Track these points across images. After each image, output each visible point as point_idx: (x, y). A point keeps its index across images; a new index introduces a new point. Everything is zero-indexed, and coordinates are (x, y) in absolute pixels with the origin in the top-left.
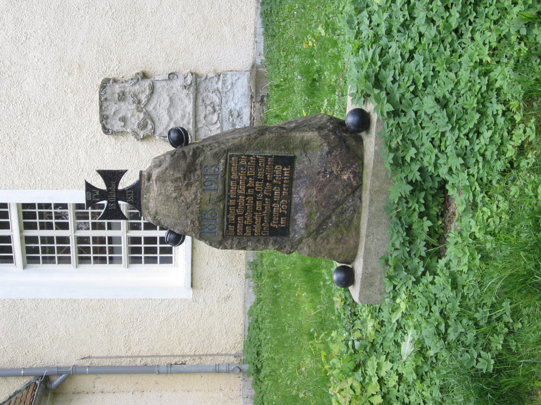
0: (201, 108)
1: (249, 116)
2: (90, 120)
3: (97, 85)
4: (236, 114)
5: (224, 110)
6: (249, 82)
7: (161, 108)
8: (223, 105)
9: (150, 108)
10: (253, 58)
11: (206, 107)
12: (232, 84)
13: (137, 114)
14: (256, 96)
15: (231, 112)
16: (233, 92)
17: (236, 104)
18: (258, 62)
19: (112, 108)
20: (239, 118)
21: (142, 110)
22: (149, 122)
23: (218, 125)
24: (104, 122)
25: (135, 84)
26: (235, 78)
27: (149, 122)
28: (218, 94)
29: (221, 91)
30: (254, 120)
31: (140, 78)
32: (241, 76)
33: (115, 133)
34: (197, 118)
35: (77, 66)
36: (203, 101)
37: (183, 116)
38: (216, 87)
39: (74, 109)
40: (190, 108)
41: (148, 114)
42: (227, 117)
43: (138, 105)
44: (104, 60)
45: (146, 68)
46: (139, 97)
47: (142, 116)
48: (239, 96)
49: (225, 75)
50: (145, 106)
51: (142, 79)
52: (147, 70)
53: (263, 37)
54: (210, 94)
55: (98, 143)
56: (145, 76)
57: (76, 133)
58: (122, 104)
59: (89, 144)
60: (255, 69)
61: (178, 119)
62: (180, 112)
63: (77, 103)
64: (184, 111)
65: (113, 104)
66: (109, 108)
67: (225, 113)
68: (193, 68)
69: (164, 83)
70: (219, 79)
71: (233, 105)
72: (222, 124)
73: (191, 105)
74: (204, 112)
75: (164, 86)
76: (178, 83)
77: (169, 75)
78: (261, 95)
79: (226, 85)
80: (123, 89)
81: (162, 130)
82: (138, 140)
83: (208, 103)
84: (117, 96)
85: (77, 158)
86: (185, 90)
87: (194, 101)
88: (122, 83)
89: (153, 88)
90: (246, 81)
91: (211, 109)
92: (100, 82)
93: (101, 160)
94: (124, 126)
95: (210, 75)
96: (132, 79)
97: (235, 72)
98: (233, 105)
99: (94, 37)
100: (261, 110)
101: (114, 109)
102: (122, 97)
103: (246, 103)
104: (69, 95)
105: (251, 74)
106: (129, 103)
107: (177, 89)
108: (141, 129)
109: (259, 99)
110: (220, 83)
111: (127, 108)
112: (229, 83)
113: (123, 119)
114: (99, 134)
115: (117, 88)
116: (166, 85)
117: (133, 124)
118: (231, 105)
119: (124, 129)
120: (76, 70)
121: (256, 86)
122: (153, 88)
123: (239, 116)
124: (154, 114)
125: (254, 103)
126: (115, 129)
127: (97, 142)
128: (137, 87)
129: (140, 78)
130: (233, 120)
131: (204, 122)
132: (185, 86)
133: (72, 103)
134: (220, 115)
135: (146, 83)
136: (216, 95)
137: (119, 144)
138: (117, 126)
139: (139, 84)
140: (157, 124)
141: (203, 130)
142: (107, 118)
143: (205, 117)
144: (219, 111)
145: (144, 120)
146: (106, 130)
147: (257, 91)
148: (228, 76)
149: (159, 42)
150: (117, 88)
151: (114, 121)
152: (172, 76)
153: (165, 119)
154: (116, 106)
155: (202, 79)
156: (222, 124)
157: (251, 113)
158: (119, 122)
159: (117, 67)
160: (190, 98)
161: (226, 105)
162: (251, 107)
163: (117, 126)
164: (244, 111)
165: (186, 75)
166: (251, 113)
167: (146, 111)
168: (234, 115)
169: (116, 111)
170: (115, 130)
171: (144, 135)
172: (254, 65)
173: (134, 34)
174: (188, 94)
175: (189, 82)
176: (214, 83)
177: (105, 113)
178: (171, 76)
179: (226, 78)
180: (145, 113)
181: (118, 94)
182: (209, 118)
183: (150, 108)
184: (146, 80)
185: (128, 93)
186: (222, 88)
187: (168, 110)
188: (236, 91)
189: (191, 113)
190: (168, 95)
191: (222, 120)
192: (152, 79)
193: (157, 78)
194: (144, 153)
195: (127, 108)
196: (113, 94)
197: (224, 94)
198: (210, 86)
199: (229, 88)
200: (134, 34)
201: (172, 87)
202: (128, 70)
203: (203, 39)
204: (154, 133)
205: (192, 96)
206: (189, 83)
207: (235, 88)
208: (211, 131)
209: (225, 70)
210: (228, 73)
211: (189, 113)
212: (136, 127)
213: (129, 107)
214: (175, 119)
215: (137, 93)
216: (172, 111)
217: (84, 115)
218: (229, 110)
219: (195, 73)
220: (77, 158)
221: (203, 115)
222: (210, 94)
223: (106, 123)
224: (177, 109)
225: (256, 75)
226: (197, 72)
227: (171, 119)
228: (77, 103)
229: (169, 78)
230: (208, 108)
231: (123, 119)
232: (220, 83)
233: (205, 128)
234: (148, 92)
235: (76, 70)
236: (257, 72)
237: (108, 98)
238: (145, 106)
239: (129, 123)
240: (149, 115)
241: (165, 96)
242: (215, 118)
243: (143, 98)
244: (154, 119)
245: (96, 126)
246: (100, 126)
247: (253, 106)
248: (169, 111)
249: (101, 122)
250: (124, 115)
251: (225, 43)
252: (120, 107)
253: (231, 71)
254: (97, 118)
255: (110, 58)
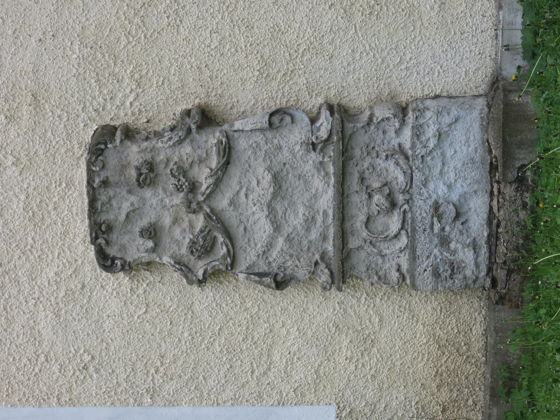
0: (357, 199)
1: (485, 216)
2: (66, 233)
3: (80, 144)
4: (450, 211)
5: (418, 202)
6: (485, 129)
7: (250, 202)
8: (415, 190)
9: (222, 202)
10: (495, 60)
11: (370, 196)
12: (440, 136)
13: (186, 218)
14: (505, 167)
15: (436, 206)
16: (443, 155)
17: (450, 187)
18: (510, 72)
19: (122, 205)
20: (458, 224)
21: (201, 208)
22: (220, 239)
23: (404, 240)
24: (101, 241)
25: (180, 142)
26: (447, 119)
27: (220, 239)
28: (402, 161)
29: (410, 153)
30: (498, 226)
31: (193, 127)
32: (462, 113)
33: (128, 267)
34: (348, 225)
35: (29, 98)
36: (362, 180)
37: (310, 222)
38: (395, 142)
39: (21, 205)
40: (327, 200)
41: (216, 219)
42: (427, 222)
43: (191, 196)
44: (98, 81)
45: (208, 95)
46: (191, 174)
47: (200, 221)
48: (459, 166)
49: (420, 112)
50: (209, 197)
51: (200, 127)
52: (213, 101)
53: (520, 8)
54: (381, 163)
55: (87, 289)
56: (207, 117)
57: (28, 265)
58: (148, 193)
59: (62, 294)
60: (500, 95)
61: (295, 228)
62: (301, 210)
63: (31, 190)
64: (310, 207)
65: (124, 193)
66: (114, 203)
67: (422, 209)
68: (333, 92)
69: (259, 138)
70: (403, 122)
71: (442, 190)
72: (412, 238)
73: (331, 192)
74: (365, 210)
75: (258, 145)
76: (295, 136)
77: (272, 115)
78: (518, 164)
79: (423, 139)
80: (148, 156)
81: (254, 258)
82: (190, 282)
83: (376, 185)
84: (133, 173)
85: (32, 328)
86: (313, 154)
87: (337, 182)
88: (147, 139)
89: (227, 152)
90: (476, 126)
91: (383, 200)
92: (88, 136)
93: (94, 332)
94: (154, 250)
95: (381, 113)
96: (173, 129)
97: (446, 100)
98: (442, 190)
99: (70, 21)
100: (519, 202)
101: (126, 207)
102: (148, 175)
103: (478, 182)
104: (9, 172)
105: (489, 106)
106: (165, 190)
107: (292, 151)
108: (199, 257)
109: (512, 175)
110: (407, 133)
111: (162, 203)
112: (431, 131)
113: (152, 232)
114: (87, 268)
115: (134, 153)
116: (262, 143)
117: (178, 243)
118: (438, 189)
119: (154, 257)
120: (25, 107)
121: (504, 141)
122: (227, 152)
123: (458, 215)
124: (231, 217)
125: (498, 182)
126: (132, 256)
127: (83, 286)
128: (186, 149)
129: (193, 127)
130: (443, 229)
131: (364, 233)
132: (313, 144)
133: (17, 190)
134: (409, 215)
135: (212, 139)
136: (397, 164)
137: (141, 291)
138: (136, 248)
139: (192, 141)
140: (241, 242)
141: (363, 254)
142: (110, 228)
143: (367, 223)
144: (406, 206)
145: (206, 232)
146: (106, 261)
147: (507, 154)
148: (428, 114)
149: (243, 29)
150: (134, 153)
151: (125, 239)
152: (278, 117)
153: (262, 228)
154: (133, 199)
155: (359, 125)
156: (412, 238)
157: (491, 208)
158: (140, 241)
159: (133, 95)
160: (327, 174)
161: (424, 190)
162: (492, 194)
163: (136, 248)
164: (472, 205)
165: (315, 111)
166: (491, 208)
167: (212, 210)
168: (445, 216)
169: (133, 211)
170: (129, 259)
171: (205, 271)
172: (496, 82)
173: (176, 12)
174: (321, 163)
175: (323, 134)
176: (392, 134)
177: (103, 217)
178: (276, 119)
179: (421, 121)
180: (208, 217)
181: (138, 169)
182: (379, 223)
183: (222, 202)
184: (209, 130)
185: (162, 166)
186: (413, 147)
187: (269, 206)
188: (449, 153)
189: (330, 212)
190: (269, 169)
191: (414, 230)
192: (226, 127)
193: (238, 125)
194: (206, 313)
195: (162, 203)
196: (124, 167)
197: (418, 162)
198: (379, 141)
199: (431, 145)
200: (176, 12)
201: (280, 148)
202: (162, 104)
203: (358, 17)
204: (233, 265)
205: (331, 169)
206: (325, 136)
207: (446, 144)
208: (383, 256)
209: (419, 94)
210: (428, 103)
211: (325, 212)
212: (184, 250)
213: (167, 200)
214: (287, 229)
215: (187, 166)
216: (279, 208)
217: (48, 221)
218: (430, 202)
219: (339, 105)
220: (32, 328)
221: (362, 218)
222: (381, 163)
223: (107, 243)
224: (292, 204)
225: (505, 113)
226: (344, 102)
227: (277, 228)
228: (31, 190)
229: (271, 124)
230: (377, 198)
231: (152, 232)
232: (407, 133)
233: (369, 248)
234: (214, 162)
235: (25, 107)
236: (507, 104)
237: (111, 179)
238: (209, 197)
239: (166, 241)
240: (219, 220)
241: (261, 170)
242: (394, 223)
243: (203, 177)
244: (232, 231)
245: (81, 248)
246: (92, 254)
247: (495, 191)
248: (271, 208)
249: (94, 240)
250: (153, 220)
251: (418, 24)
252: (143, 200)
253: (437, 97)
254: (82, 226)
255: (113, 74)
